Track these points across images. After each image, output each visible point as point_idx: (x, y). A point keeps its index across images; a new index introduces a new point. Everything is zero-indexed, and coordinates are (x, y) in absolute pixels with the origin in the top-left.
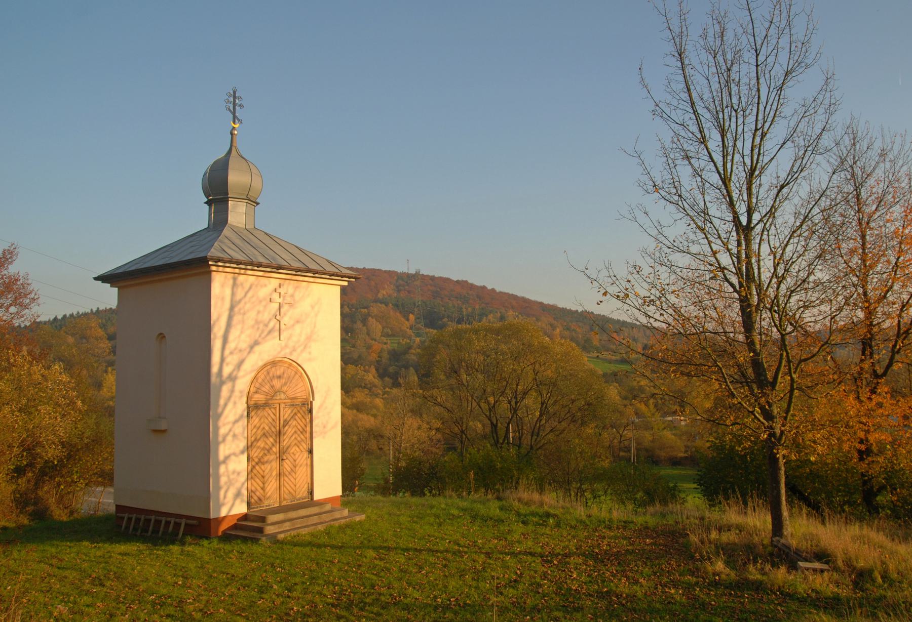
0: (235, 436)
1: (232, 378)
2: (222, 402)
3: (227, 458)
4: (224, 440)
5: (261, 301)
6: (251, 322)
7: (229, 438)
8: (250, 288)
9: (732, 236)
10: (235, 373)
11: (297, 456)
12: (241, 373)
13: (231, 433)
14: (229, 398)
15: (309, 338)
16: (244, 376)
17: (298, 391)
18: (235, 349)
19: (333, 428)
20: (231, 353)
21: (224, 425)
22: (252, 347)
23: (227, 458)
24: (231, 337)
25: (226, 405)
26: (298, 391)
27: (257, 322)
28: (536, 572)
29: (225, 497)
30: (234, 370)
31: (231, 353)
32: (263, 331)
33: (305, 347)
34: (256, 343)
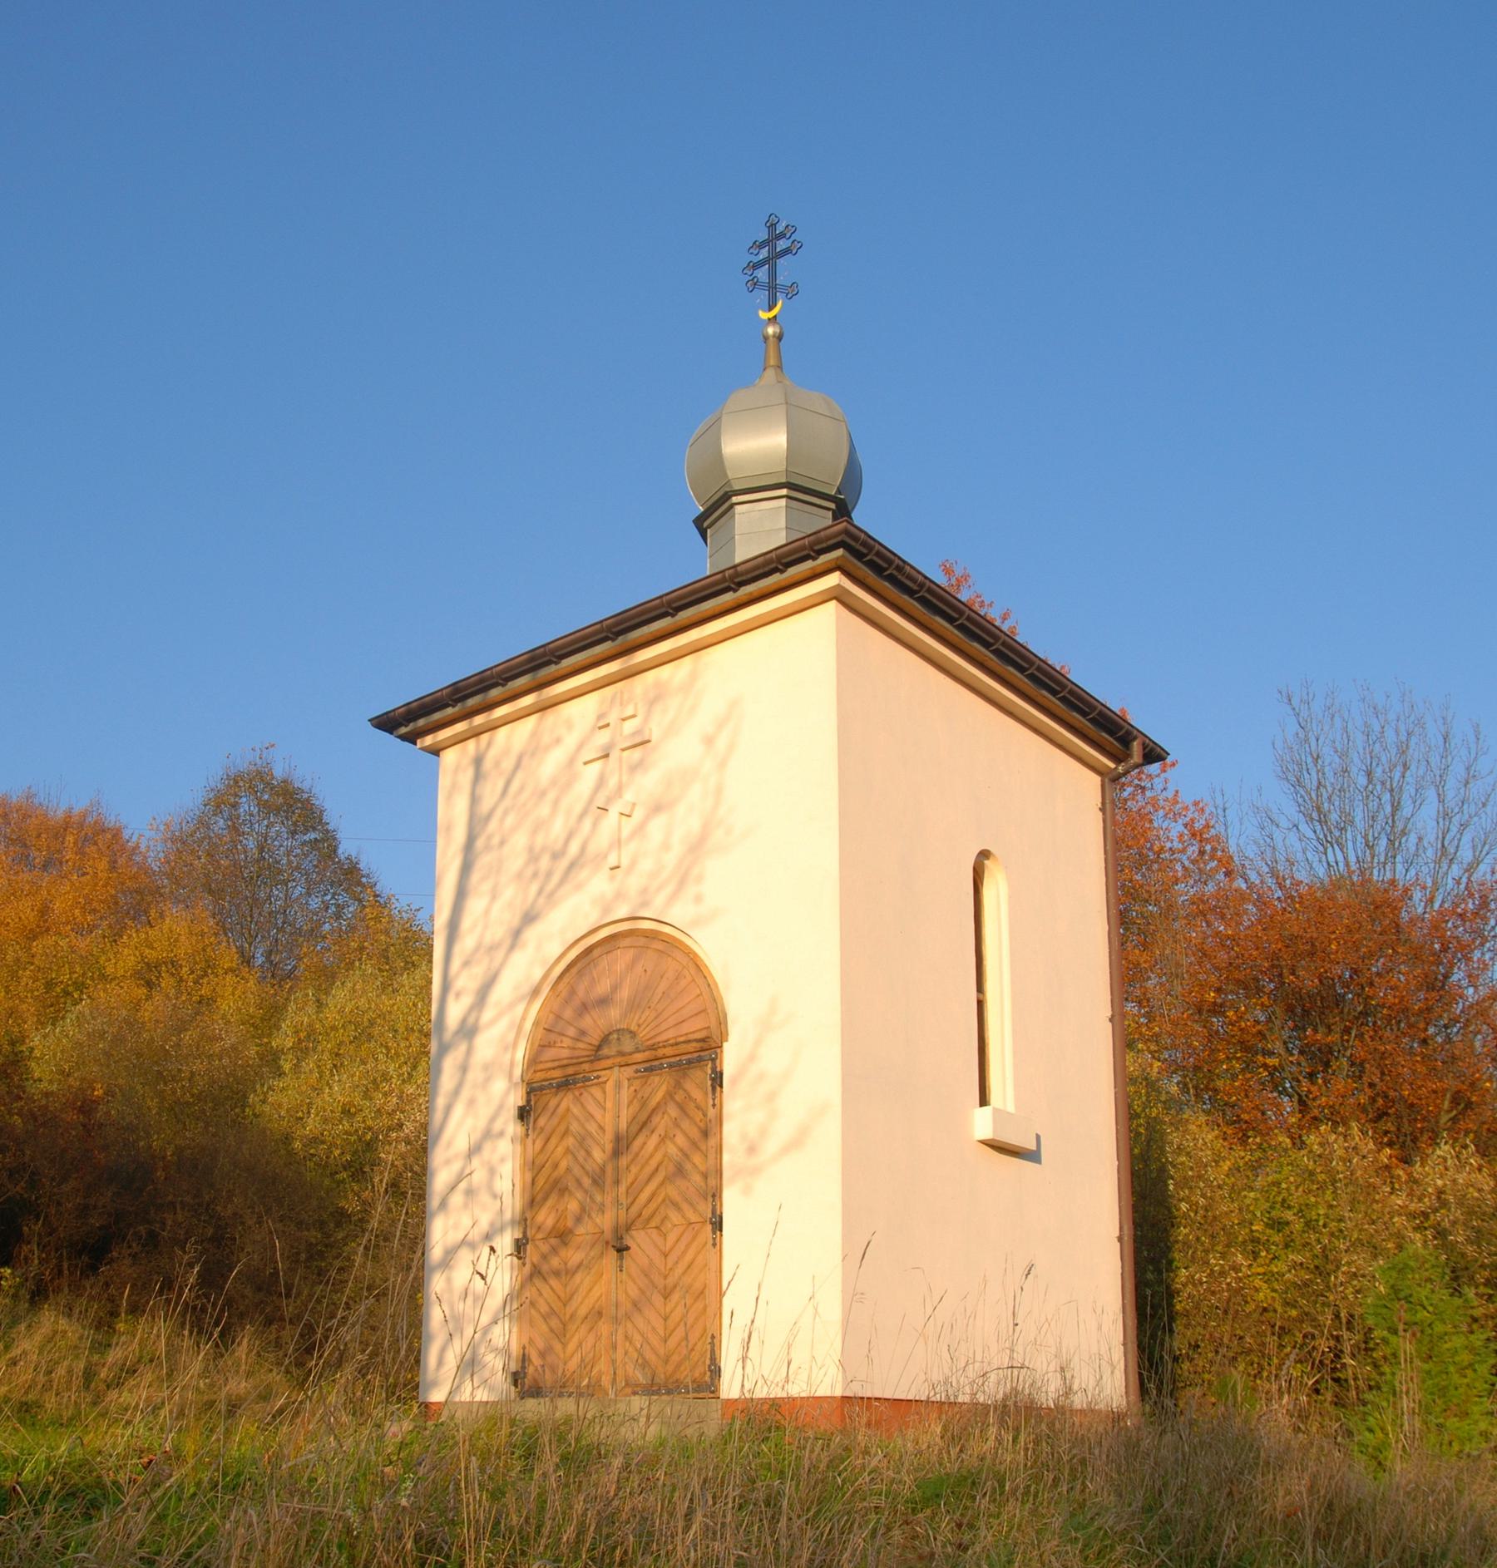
0: (470, 1193)
1: (468, 1031)
2: (441, 1102)
3: (450, 1253)
4: (443, 1204)
5: (543, 794)
6: (515, 863)
7: (457, 1199)
8: (518, 766)
9: (1408, 784)
10: (471, 1020)
11: (672, 1238)
12: (487, 1015)
13: (463, 1185)
14: (457, 1092)
15: (697, 847)
16: (493, 1022)
17: (664, 1026)
18: (477, 949)
19: (796, 1143)
20: (466, 964)
21: (448, 1162)
22: (517, 934)
23: (450, 1253)
24: (466, 923)
25: (448, 1109)
26: (664, 1026)
27: (533, 857)
28: (198, 1515)
29: (440, 1363)
30: (471, 1009)
31: (466, 964)
32: (549, 874)
33: (682, 883)
34: (529, 918)
